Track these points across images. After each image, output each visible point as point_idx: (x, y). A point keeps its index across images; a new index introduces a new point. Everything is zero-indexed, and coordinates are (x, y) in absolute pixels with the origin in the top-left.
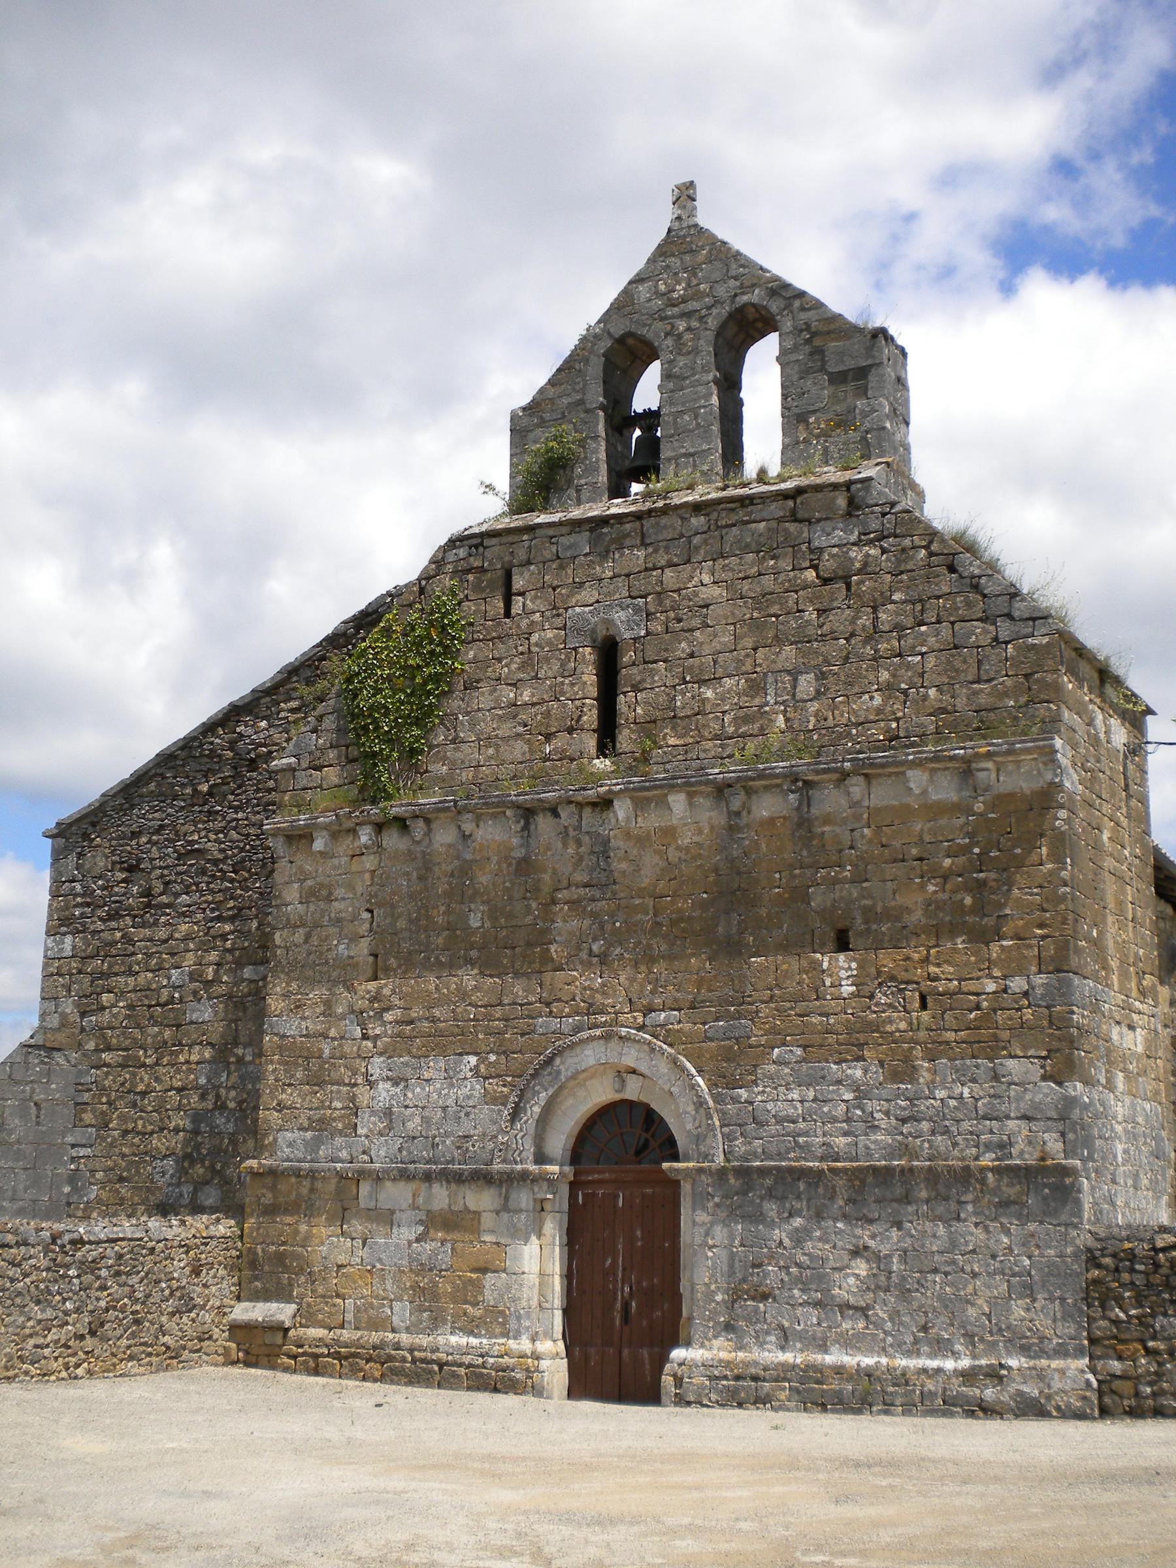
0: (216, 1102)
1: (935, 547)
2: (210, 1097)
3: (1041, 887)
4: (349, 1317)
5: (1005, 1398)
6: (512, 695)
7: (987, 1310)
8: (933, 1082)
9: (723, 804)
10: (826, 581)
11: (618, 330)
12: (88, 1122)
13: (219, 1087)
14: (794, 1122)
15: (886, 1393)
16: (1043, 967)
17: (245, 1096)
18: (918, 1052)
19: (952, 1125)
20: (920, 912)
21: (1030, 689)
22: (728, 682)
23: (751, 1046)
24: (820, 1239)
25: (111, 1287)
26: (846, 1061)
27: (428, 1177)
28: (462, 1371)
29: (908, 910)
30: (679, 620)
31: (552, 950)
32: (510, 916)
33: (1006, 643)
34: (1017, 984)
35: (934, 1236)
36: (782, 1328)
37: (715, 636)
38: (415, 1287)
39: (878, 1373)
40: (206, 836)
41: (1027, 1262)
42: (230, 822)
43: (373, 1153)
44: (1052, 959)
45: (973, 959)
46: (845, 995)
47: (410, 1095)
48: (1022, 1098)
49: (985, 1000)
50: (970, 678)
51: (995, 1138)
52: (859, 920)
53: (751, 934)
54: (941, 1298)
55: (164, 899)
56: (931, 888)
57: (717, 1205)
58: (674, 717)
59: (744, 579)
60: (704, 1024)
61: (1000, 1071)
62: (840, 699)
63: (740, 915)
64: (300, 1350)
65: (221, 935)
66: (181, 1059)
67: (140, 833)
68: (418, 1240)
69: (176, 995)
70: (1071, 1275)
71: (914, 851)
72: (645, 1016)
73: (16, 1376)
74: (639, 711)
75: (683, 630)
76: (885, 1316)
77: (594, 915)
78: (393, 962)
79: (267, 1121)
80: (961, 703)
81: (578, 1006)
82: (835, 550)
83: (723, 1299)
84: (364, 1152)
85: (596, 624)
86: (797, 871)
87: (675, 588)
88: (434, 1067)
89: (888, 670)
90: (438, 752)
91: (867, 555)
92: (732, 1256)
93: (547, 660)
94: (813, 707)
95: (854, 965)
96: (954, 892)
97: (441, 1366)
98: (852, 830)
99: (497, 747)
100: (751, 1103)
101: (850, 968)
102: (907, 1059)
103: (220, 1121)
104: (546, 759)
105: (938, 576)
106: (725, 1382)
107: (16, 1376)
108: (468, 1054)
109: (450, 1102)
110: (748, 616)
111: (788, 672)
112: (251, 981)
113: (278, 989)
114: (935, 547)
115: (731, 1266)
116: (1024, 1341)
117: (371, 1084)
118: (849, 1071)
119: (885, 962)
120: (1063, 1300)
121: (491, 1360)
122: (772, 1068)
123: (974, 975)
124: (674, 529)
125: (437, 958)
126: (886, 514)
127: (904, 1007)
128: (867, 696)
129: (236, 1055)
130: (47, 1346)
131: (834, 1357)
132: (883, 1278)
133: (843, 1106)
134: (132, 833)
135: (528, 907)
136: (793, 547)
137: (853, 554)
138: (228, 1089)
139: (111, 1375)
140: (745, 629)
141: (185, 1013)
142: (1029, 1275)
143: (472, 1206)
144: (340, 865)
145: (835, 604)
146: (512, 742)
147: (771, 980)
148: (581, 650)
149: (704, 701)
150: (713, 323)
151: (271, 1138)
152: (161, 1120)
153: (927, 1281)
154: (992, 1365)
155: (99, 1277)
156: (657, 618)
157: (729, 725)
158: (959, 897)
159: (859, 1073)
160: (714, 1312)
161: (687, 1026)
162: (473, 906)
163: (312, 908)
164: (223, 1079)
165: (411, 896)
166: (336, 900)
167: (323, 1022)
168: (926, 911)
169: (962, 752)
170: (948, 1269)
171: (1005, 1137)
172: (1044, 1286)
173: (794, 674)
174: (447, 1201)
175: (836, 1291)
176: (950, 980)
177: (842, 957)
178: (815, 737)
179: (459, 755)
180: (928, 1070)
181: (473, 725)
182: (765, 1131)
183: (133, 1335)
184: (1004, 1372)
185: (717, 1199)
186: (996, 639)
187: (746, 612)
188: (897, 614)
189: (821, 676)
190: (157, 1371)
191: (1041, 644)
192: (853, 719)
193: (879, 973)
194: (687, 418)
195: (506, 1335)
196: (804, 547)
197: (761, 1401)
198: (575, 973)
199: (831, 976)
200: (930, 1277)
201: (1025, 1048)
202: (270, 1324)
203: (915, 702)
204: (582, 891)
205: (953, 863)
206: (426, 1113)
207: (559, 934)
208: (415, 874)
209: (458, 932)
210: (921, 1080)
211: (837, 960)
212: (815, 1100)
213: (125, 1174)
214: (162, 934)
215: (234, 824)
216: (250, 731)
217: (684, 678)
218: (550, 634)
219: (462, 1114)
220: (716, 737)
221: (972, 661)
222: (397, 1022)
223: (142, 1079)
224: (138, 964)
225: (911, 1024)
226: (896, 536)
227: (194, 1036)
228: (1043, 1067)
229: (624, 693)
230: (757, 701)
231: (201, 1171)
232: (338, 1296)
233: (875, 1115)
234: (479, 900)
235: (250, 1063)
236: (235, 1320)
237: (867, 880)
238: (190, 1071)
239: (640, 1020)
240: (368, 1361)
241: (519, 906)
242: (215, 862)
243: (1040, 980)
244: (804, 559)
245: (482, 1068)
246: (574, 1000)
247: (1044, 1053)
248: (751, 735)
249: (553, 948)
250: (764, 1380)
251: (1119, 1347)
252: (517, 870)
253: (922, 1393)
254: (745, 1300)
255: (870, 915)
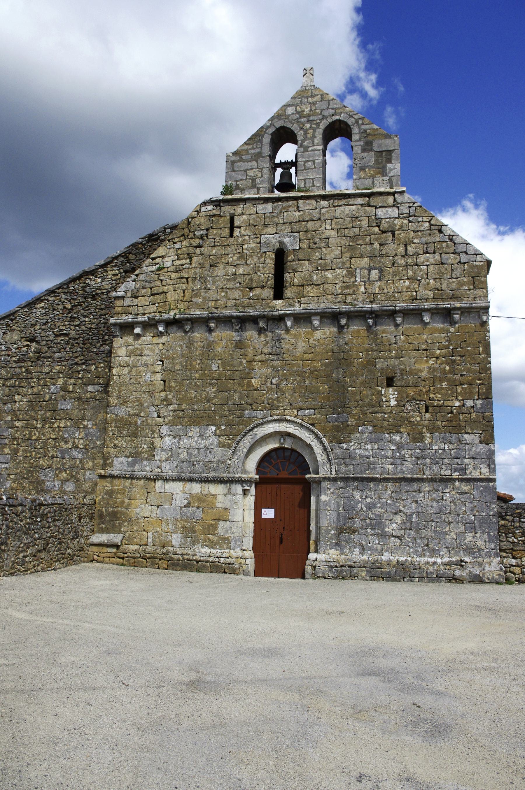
0: (73, 445)
1: (433, 222)
2: (70, 443)
3: (479, 364)
4: (150, 540)
5: (464, 574)
6: (234, 270)
7: (455, 537)
8: (432, 443)
9: (336, 322)
10: (384, 232)
11: (278, 124)
12: (6, 453)
13: (74, 438)
14: (368, 458)
15: (411, 572)
16: (480, 397)
17: (88, 443)
18: (424, 430)
19: (440, 461)
20: (426, 372)
21: (474, 283)
22: (338, 271)
23: (348, 426)
24: (380, 507)
25: (52, 527)
26: (392, 433)
27: (191, 480)
28: (208, 564)
29: (421, 371)
30: (315, 244)
31: (253, 382)
32: (232, 366)
33: (464, 263)
34: (469, 403)
35: (432, 506)
36: (362, 546)
37: (332, 251)
38: (184, 527)
39: (407, 564)
40: (69, 328)
41: (473, 518)
42: (82, 322)
43: (162, 468)
44: (484, 393)
45: (449, 392)
46: (392, 405)
47: (181, 443)
48: (471, 450)
49: (455, 409)
50: (448, 277)
51: (459, 466)
52: (399, 374)
53: (348, 378)
54: (435, 532)
55: (48, 354)
56: (431, 362)
57: (332, 493)
58: (313, 284)
59: (345, 229)
60: (326, 415)
61: (461, 439)
62: (390, 281)
63: (343, 370)
64: (126, 555)
65: (77, 372)
66: (55, 425)
67: (35, 325)
68: (185, 507)
69: (53, 397)
70: (492, 523)
71: (424, 347)
72: (298, 411)
73: (15, 572)
74: (296, 280)
75: (317, 248)
76: (409, 540)
77: (273, 367)
78: (173, 384)
79: (109, 453)
80: (444, 286)
81: (265, 406)
82: (388, 220)
83: (334, 533)
84: (158, 467)
85: (275, 242)
86: (370, 352)
87: (313, 230)
88: (195, 431)
89: (412, 271)
90: (197, 293)
91: (402, 223)
92: (339, 515)
93: (252, 256)
94: (378, 284)
95: (396, 393)
96: (441, 364)
97: (197, 562)
98: (395, 336)
99: (226, 293)
100: (349, 450)
101: (394, 394)
102: (421, 433)
103: (75, 453)
104: (249, 299)
105: (434, 234)
106: (336, 568)
107: (15, 572)
108: (212, 425)
109: (201, 446)
110: (347, 244)
111: (366, 269)
112: (92, 392)
113: (115, 394)
114: (433, 222)
115: (338, 519)
116: (472, 550)
117: (162, 437)
118: (394, 437)
119: (410, 392)
120: (489, 533)
121: (222, 560)
122: (358, 435)
123: (450, 399)
124: (313, 205)
125: (195, 383)
126: (412, 207)
127: (419, 411)
128: (402, 281)
129: (84, 425)
130: (28, 556)
131: (387, 556)
132: (408, 524)
133: (391, 452)
134: (32, 325)
135: (241, 362)
136: (368, 217)
137: (395, 222)
138: (79, 439)
139: (50, 569)
140: (346, 249)
141: (57, 405)
142: (474, 523)
143: (213, 492)
144: (147, 340)
145: (388, 242)
146: (234, 290)
147: (358, 398)
148: (268, 253)
149: (327, 278)
150: (322, 126)
151: (110, 460)
152: (45, 452)
153: (428, 525)
154: (457, 560)
155: (48, 522)
156: (304, 242)
157: (339, 289)
158: (443, 366)
159: (398, 438)
160: (330, 539)
161: (318, 417)
162: (213, 361)
163: (132, 359)
164: (76, 435)
165: (183, 356)
166: (144, 355)
167: (137, 410)
168: (429, 372)
169: (449, 306)
170: (437, 520)
171: (463, 466)
172: (480, 528)
173: (370, 270)
174: (200, 490)
175: (387, 530)
176: (440, 401)
177: (391, 389)
178: (379, 297)
179: (207, 295)
180: (429, 438)
181: (214, 282)
182: (355, 462)
183: (59, 549)
184: (463, 563)
185: (332, 490)
186: (460, 262)
187: (344, 242)
188: (416, 248)
189: (381, 271)
190: (66, 566)
191: (479, 265)
192: (396, 290)
193: (407, 396)
194: (310, 163)
195: (228, 548)
196: (373, 217)
197: (353, 577)
198: (264, 392)
199: (386, 397)
200: (430, 523)
201: (472, 429)
202: (111, 544)
203: (423, 285)
204: (267, 356)
205: (441, 352)
206: (190, 451)
207: (256, 375)
208: (185, 346)
209: (206, 372)
210: (426, 442)
211: (389, 390)
212: (378, 449)
213: (25, 476)
214: (47, 370)
215: (84, 323)
216: (93, 283)
217: (317, 268)
218: (253, 245)
219: (208, 452)
220: (333, 294)
221: (449, 270)
222: (175, 410)
223: (35, 434)
224: (34, 382)
225: (421, 418)
226: (415, 216)
227: (62, 415)
228: (480, 437)
229: (289, 273)
230: (352, 280)
231: (65, 475)
232: (145, 531)
233: (405, 456)
234: (217, 358)
235: (91, 428)
236: (92, 542)
237: (402, 357)
238: (60, 430)
239: (296, 413)
240: (160, 559)
241: (237, 362)
242: (75, 339)
243: (479, 402)
244: (373, 222)
245: (218, 432)
246: (263, 403)
247: (480, 432)
248: (349, 294)
249: (253, 381)
250: (354, 567)
251: (514, 553)
252: (235, 346)
253: (427, 572)
254: (345, 533)
255: (403, 372)
